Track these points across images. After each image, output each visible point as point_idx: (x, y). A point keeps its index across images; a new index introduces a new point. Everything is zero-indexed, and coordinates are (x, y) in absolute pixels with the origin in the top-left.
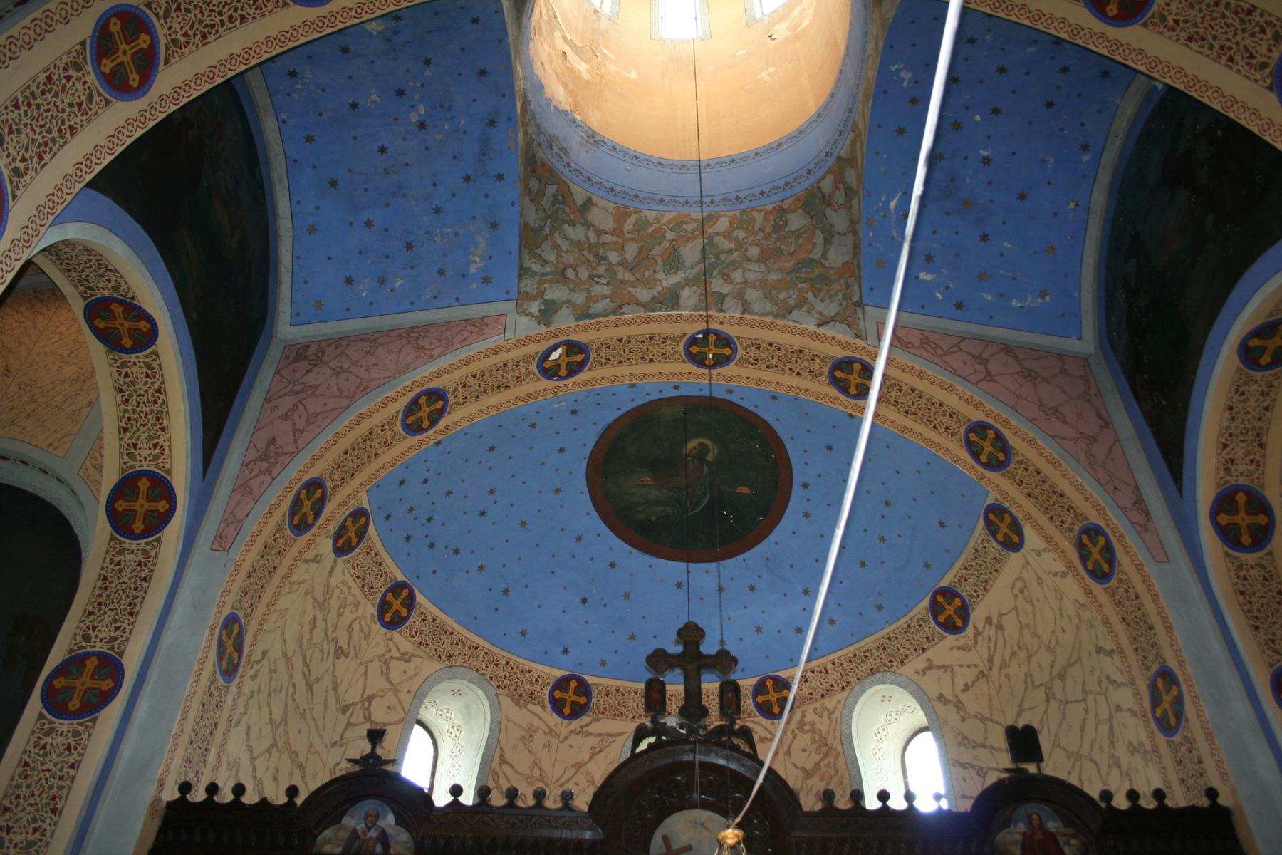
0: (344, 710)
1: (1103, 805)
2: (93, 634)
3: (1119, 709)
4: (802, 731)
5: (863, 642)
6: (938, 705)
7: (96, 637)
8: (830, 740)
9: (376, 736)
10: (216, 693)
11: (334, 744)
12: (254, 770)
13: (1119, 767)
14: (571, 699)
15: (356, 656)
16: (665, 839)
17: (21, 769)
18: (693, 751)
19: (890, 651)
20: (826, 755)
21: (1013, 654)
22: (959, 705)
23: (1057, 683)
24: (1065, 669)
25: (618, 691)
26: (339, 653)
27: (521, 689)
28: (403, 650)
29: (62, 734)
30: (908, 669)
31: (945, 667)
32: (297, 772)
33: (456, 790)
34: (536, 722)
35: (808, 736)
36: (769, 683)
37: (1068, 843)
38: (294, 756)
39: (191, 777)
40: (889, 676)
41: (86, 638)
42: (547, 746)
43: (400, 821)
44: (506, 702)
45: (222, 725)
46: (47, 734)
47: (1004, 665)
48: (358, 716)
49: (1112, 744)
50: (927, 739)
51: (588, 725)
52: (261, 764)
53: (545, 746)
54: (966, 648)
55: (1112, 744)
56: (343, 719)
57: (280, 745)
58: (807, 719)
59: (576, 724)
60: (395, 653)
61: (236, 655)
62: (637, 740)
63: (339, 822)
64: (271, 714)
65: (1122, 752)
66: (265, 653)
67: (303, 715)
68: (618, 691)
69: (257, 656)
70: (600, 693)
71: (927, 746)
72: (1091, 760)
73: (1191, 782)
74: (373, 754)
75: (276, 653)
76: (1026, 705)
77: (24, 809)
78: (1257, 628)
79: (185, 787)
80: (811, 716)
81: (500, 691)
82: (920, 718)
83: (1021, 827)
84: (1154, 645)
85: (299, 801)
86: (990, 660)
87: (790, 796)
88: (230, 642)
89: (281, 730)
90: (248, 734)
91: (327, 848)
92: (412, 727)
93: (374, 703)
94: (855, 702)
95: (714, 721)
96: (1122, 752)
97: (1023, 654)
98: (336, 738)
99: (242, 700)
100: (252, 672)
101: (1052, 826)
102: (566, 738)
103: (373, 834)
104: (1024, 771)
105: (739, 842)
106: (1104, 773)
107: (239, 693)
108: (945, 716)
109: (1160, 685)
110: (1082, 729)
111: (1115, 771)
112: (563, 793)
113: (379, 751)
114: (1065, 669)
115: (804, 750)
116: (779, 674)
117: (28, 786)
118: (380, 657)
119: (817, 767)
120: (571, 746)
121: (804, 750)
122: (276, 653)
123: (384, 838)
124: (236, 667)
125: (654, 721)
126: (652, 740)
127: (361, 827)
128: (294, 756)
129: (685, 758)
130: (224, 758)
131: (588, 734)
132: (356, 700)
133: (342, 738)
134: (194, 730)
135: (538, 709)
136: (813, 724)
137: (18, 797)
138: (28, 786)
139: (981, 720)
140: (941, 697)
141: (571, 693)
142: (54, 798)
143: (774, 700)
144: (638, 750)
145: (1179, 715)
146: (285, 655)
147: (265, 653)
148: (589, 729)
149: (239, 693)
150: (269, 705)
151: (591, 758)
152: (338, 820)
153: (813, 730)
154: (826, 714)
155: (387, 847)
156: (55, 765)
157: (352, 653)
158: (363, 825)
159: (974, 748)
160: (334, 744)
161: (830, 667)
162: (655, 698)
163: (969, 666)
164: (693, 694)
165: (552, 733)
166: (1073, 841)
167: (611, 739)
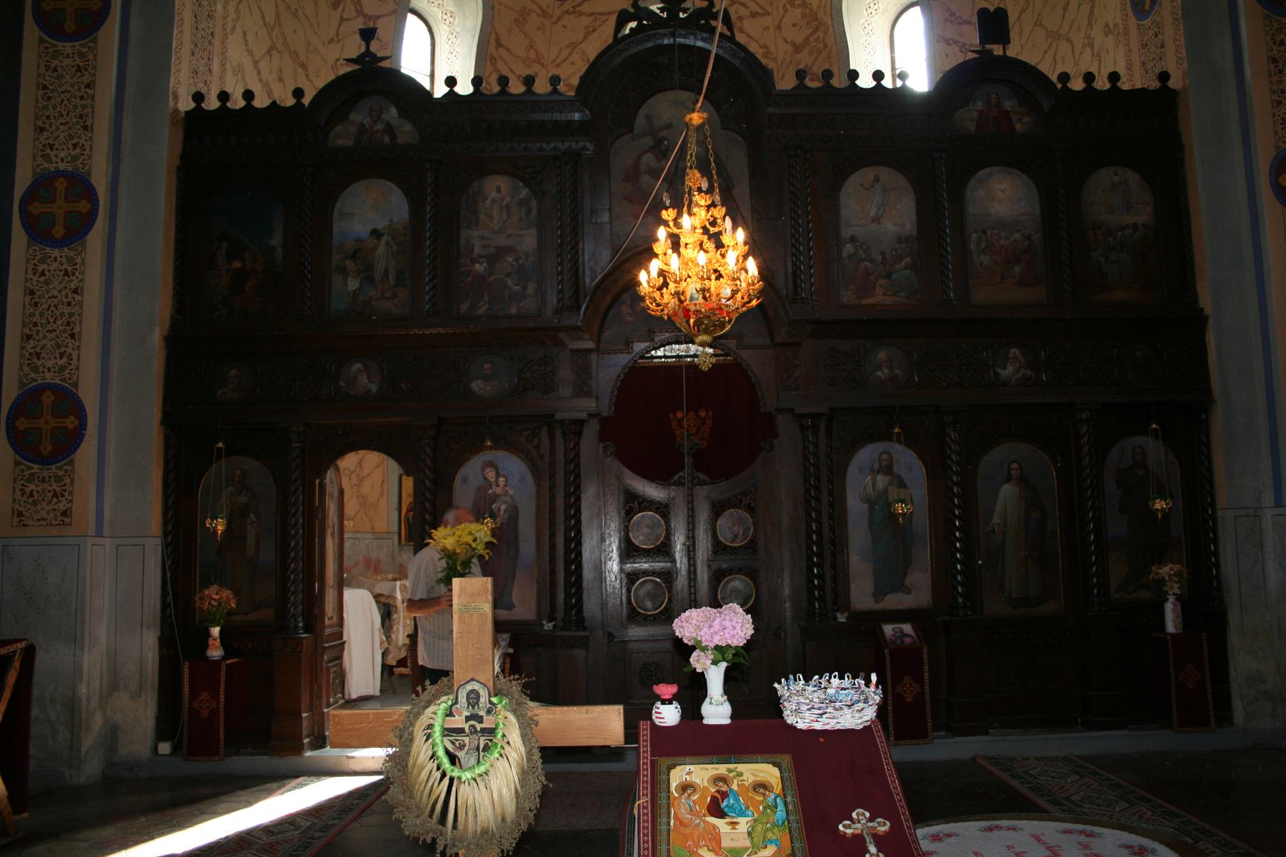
1: (1059, 86)
8: (821, 14)
9: (368, 34)
11: (331, 41)
12: (259, 73)
13: (1092, 47)
16: (649, 118)
20: (816, 30)
29: (68, 56)
32: (300, 70)
33: (451, 81)
35: (798, 11)
38: (294, 55)
42: (541, 28)
43: (402, 113)
49: (1090, 25)
52: (263, 66)
55: (1090, 25)
57: (279, 46)
62: (621, 23)
64: (263, 17)
65: (1097, 33)
67: (295, 14)
72: (1068, 40)
74: (368, 53)
77: (58, 129)
79: (198, 97)
83: (980, 105)
85: (306, 101)
87: (765, 75)
89: (276, 31)
90: (245, 40)
91: (340, 142)
92: (405, 17)
96: (1097, 33)
98: (333, 33)
101: (1007, 105)
102: (559, 19)
103: (379, 126)
104: (990, 52)
105: (703, 124)
106: (1077, 52)
110: (1065, 9)
113: (374, 47)
115: (794, 25)
117: (54, 107)
119: (807, 41)
120: (565, 27)
121: (794, 25)
123: (389, 129)
126: (633, 24)
127: (367, 121)
128: (294, 55)
129: (666, 42)
130: (228, 66)
131: (581, 14)
134: (192, 42)
142: (81, 116)
150: (259, 8)
156: (72, 86)
159: (960, 24)
160: (331, 41)
166: (1026, 119)
167: (604, 18)
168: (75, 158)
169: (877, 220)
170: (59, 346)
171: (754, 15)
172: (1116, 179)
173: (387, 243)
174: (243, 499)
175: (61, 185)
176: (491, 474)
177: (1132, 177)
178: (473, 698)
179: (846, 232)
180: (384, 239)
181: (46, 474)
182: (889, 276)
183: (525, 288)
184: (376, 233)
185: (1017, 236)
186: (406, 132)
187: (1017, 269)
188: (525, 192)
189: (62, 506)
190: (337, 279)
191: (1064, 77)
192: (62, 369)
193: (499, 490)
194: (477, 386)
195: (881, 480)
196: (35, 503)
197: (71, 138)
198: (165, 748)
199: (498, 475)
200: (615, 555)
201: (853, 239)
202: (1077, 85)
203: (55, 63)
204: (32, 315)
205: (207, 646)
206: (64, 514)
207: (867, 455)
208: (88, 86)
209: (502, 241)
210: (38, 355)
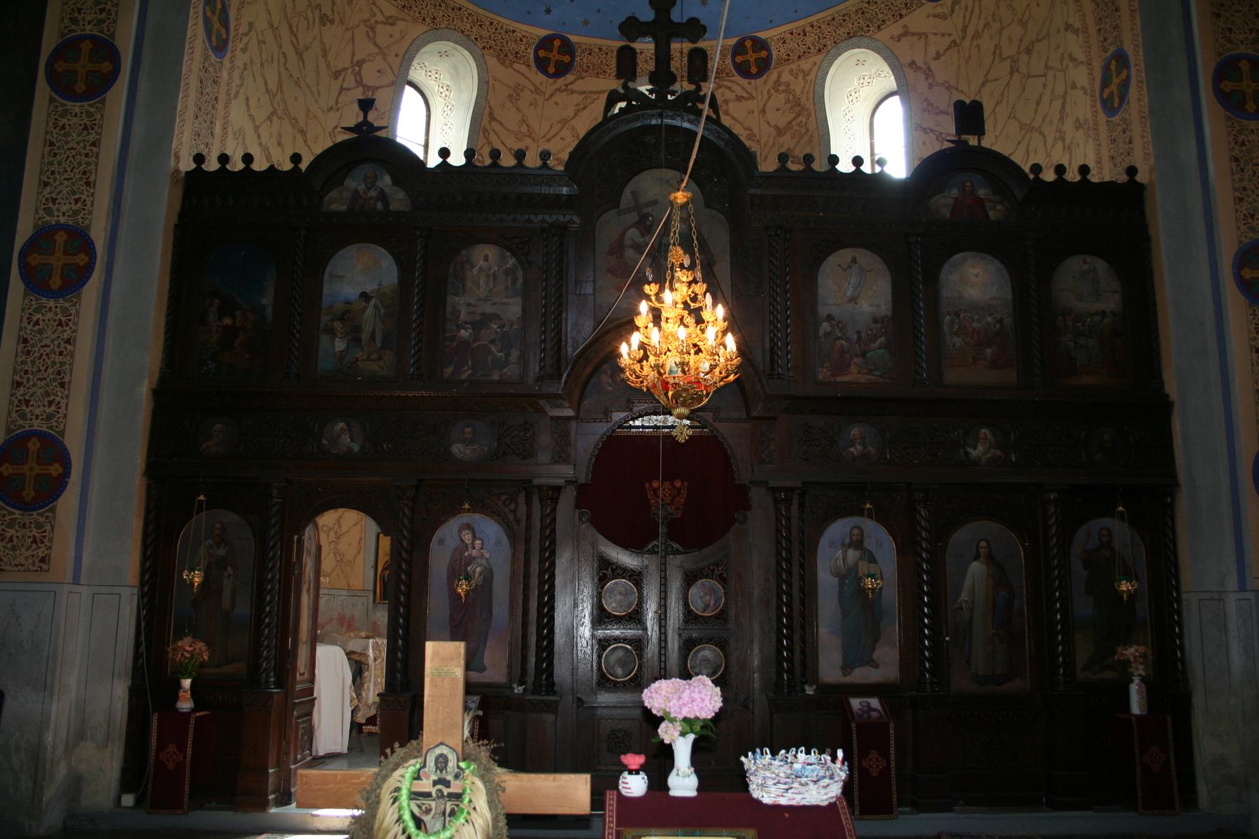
0: (336, 75)
1: (1032, 177)
2: (80, 17)
3: (1074, 86)
4: (777, 91)
5: (843, 6)
6: (909, 71)
7: (83, 19)
8: (803, 101)
9: (366, 105)
10: (211, 69)
12: (259, 137)
13: (1063, 140)
14: (556, 58)
15: (342, 22)
17: (47, 149)
18: (661, 116)
19: (868, 16)
20: (798, 115)
21: (987, 25)
22: (928, 73)
23: (1024, 57)
24: (1032, 43)
25: (600, 49)
26: (324, 20)
27: (506, 49)
28: (387, 14)
29: (76, 115)
30: (884, 35)
31: (919, 35)
32: (299, 136)
33: (444, 153)
34: (523, 81)
36: (748, 44)
37: (994, 209)
38: (294, 122)
39: (202, 149)
40: (866, 40)
41: (74, 21)
42: (533, 104)
43: (395, 182)
44: (492, 62)
45: (222, 98)
46: (63, 116)
47: (977, 36)
48: (350, 81)
49: (1061, 118)
50: (896, 100)
51: (572, 83)
52: (264, 131)
53: (531, 104)
54: (943, 17)
56: (336, 85)
57: (280, 112)
58: (782, 80)
59: (561, 82)
60: (380, 18)
61: (223, 31)
62: (610, 103)
63: (342, 184)
66: (251, 25)
67: (297, 83)
68: (600, 49)
69: (244, 28)
70: (583, 52)
71: (894, 110)
73: (1118, 160)
74: (365, 122)
75: (261, 24)
76: (991, 76)
77: (61, 184)
78: (1218, 16)
79: (199, 159)
80: (786, 77)
81: (486, 51)
82: (890, 82)
83: (955, 192)
84: (1116, 27)
85: (303, 166)
86: (964, 29)
87: (748, 158)
88: (216, 19)
89: (278, 98)
91: (334, 207)
93: (364, 66)
94: (830, 64)
95: (683, 85)
96: (1068, 126)
97: (996, 26)
98: (332, 102)
99: (236, 74)
100: (241, 46)
101: (982, 193)
102: (552, 96)
103: (373, 193)
104: (966, 142)
107: (232, 69)
108: (912, 81)
109: (1113, 68)
110: (1038, 103)
111: (1060, 144)
112: (542, 153)
114: (1032, 43)
115: (778, 110)
116: (759, 35)
118: (365, 21)
121: (778, 110)
122: (261, 24)
123: (383, 196)
124: (225, 42)
125: (625, 86)
126: (623, 104)
128: (294, 122)
129: (654, 122)
130: (230, 129)
131: (573, 92)
132: (347, 65)
133: (337, 103)
134: (197, 105)
135: (523, 68)
136: (788, 84)
137: (53, 173)
138: (60, 163)
139: (947, 88)
140: (912, 64)
141: (555, 52)
142: (85, 173)
143: (752, 60)
144: (610, 114)
145: (1123, 97)
146: (271, 25)
147: (251, 25)
148: (574, 87)
149: (232, 69)
150: (263, 75)
151: (576, 114)
152: (340, 183)
153: (788, 91)
154: (801, 75)
155: (386, 204)
156: (78, 143)
157: (337, 18)
158: (363, 186)
160: (331, 109)
161: (808, 29)
162: (626, 65)
163: (943, 35)
164: (663, 57)
165: (537, 90)
166: (999, 207)
167: (595, 96)
168: (76, 213)
169: (853, 300)
170: (48, 394)
171: (739, 99)
172: (1085, 267)
173: (376, 306)
174: (221, 552)
175: (61, 238)
176: (467, 537)
177: (1101, 266)
178: (442, 762)
179: (823, 311)
180: (372, 302)
181: (27, 520)
182: (864, 355)
183: (508, 355)
184: (365, 296)
185: (989, 319)
186: (399, 200)
187: (989, 351)
188: (511, 262)
189: (41, 552)
190: (324, 339)
191: (1037, 168)
192: (50, 417)
193: (474, 553)
194: (457, 449)
195: (852, 554)
196: (14, 549)
197: (74, 193)
198: (128, 800)
199: (474, 537)
200: (587, 621)
201: (830, 318)
202: (1049, 176)
203: (63, 121)
204: (24, 362)
205: (176, 698)
206: (43, 560)
207: (839, 529)
208: (93, 144)
209: (488, 309)
210: (27, 402)
